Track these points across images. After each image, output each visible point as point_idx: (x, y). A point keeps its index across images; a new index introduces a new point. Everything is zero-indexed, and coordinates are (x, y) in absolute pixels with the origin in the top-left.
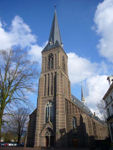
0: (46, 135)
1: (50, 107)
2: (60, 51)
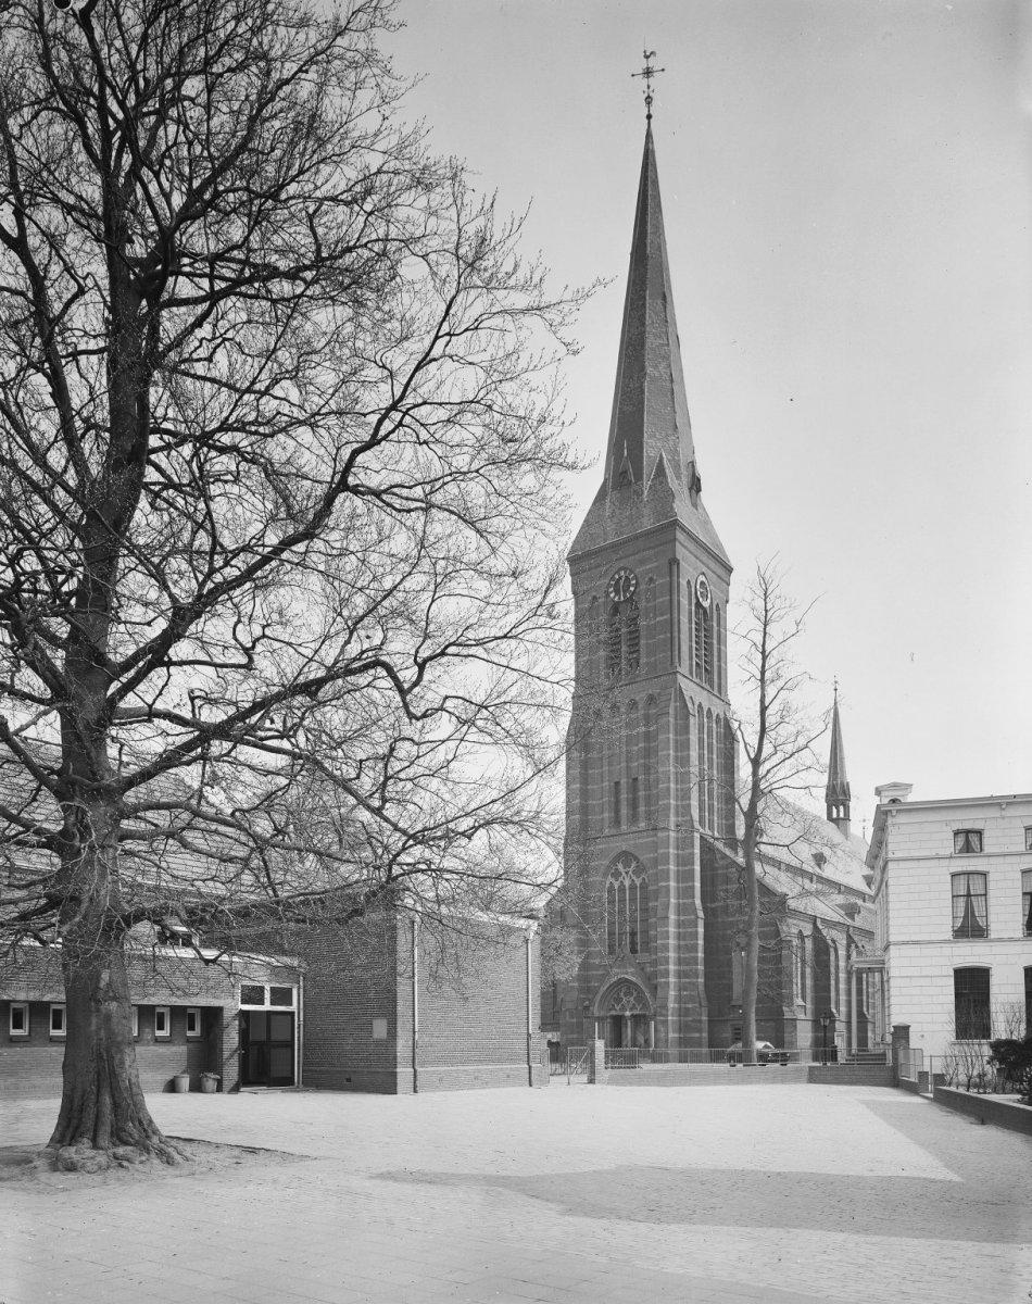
0: (613, 1013)
1: (627, 883)
2: (681, 553)
